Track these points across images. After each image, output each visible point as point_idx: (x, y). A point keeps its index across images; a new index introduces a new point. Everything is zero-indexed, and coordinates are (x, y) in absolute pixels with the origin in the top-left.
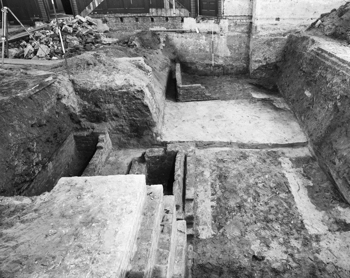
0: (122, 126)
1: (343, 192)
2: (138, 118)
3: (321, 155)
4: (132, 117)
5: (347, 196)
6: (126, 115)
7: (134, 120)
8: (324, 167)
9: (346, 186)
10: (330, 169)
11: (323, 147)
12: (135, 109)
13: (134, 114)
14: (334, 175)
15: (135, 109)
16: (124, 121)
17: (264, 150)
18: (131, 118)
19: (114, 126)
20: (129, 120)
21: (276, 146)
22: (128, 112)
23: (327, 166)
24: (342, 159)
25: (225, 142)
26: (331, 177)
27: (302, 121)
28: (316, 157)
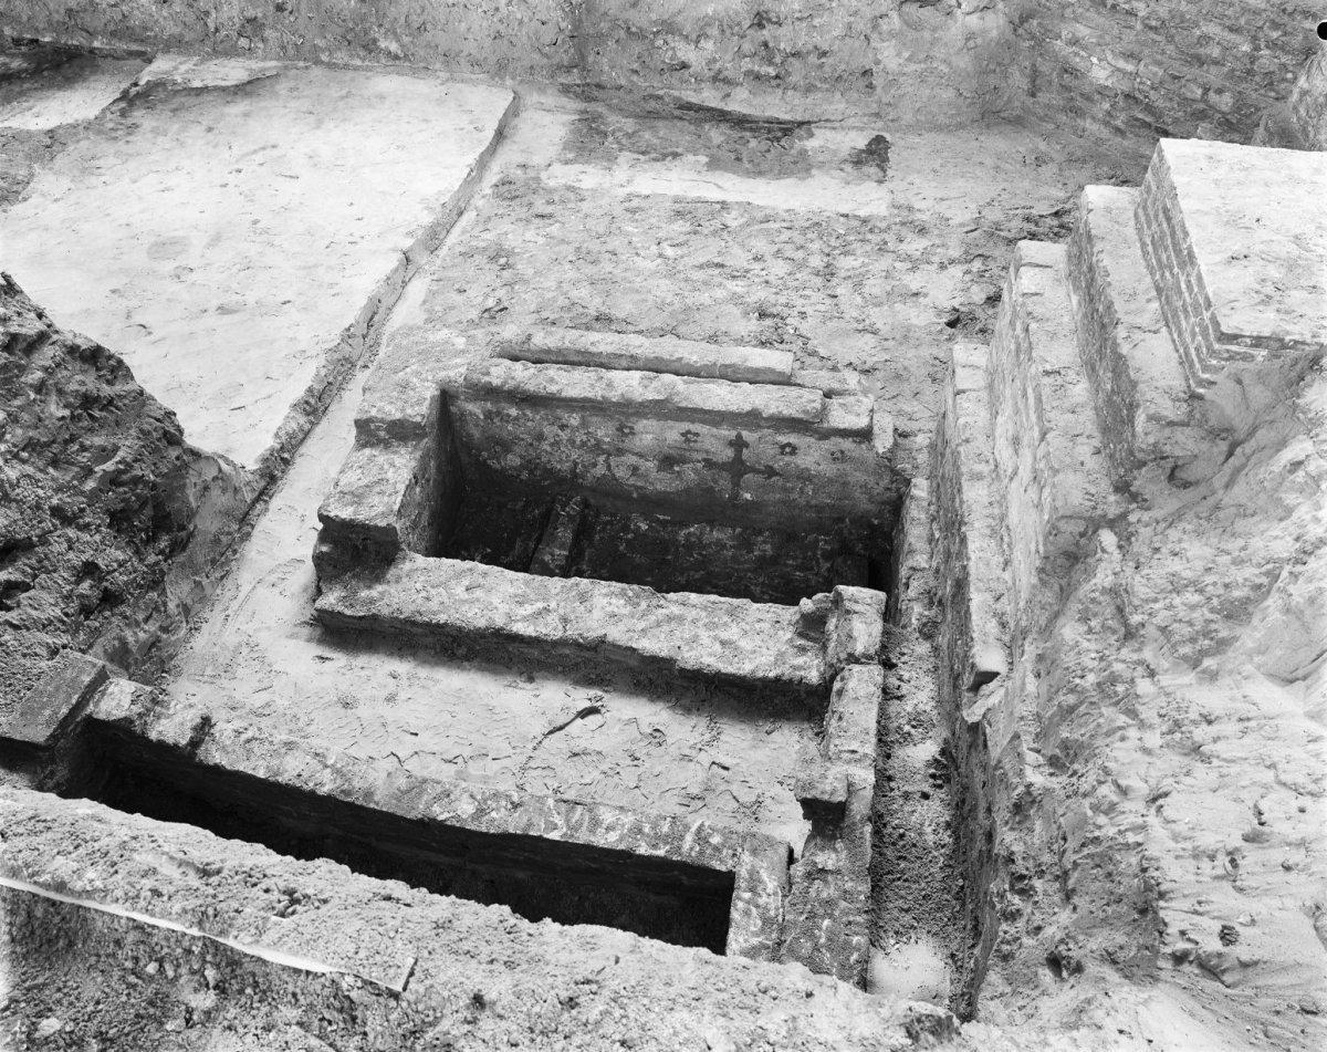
0: (89, 570)
1: (768, 114)
2: (116, 449)
3: (604, 88)
4: (89, 472)
5: (789, 108)
6: (59, 490)
7: (113, 480)
8: (652, 105)
9: (770, 90)
10: (676, 93)
11: (591, 59)
12: (67, 413)
13: (83, 448)
14: (710, 97)
15: (67, 413)
16: (71, 532)
17: (479, 202)
18: (90, 485)
19: (58, 612)
20: (93, 497)
21: (483, 163)
22: (55, 463)
23: (659, 98)
24: (709, 31)
25: (396, 270)
26: (699, 108)
27: (396, 57)
28: (592, 107)
